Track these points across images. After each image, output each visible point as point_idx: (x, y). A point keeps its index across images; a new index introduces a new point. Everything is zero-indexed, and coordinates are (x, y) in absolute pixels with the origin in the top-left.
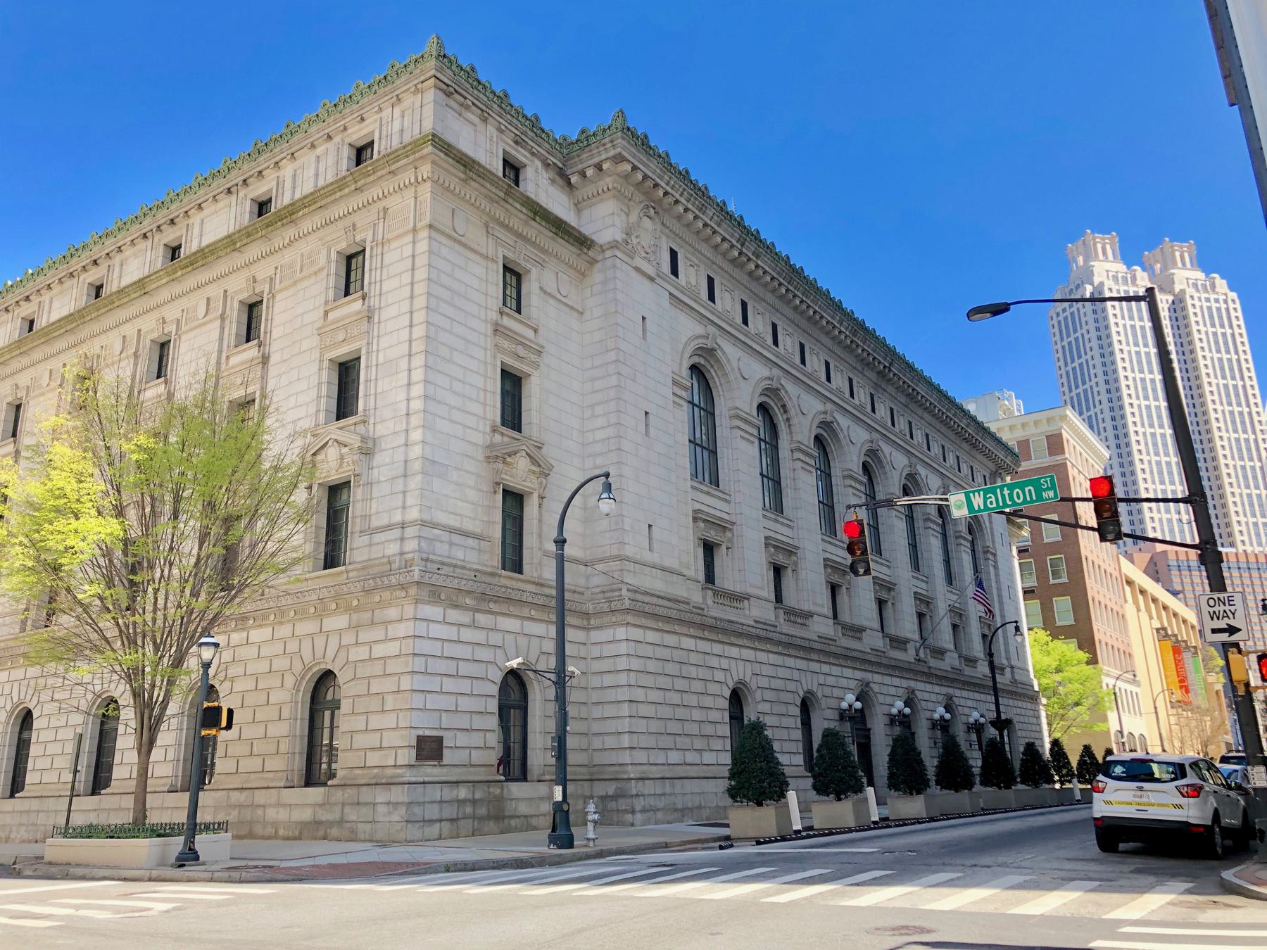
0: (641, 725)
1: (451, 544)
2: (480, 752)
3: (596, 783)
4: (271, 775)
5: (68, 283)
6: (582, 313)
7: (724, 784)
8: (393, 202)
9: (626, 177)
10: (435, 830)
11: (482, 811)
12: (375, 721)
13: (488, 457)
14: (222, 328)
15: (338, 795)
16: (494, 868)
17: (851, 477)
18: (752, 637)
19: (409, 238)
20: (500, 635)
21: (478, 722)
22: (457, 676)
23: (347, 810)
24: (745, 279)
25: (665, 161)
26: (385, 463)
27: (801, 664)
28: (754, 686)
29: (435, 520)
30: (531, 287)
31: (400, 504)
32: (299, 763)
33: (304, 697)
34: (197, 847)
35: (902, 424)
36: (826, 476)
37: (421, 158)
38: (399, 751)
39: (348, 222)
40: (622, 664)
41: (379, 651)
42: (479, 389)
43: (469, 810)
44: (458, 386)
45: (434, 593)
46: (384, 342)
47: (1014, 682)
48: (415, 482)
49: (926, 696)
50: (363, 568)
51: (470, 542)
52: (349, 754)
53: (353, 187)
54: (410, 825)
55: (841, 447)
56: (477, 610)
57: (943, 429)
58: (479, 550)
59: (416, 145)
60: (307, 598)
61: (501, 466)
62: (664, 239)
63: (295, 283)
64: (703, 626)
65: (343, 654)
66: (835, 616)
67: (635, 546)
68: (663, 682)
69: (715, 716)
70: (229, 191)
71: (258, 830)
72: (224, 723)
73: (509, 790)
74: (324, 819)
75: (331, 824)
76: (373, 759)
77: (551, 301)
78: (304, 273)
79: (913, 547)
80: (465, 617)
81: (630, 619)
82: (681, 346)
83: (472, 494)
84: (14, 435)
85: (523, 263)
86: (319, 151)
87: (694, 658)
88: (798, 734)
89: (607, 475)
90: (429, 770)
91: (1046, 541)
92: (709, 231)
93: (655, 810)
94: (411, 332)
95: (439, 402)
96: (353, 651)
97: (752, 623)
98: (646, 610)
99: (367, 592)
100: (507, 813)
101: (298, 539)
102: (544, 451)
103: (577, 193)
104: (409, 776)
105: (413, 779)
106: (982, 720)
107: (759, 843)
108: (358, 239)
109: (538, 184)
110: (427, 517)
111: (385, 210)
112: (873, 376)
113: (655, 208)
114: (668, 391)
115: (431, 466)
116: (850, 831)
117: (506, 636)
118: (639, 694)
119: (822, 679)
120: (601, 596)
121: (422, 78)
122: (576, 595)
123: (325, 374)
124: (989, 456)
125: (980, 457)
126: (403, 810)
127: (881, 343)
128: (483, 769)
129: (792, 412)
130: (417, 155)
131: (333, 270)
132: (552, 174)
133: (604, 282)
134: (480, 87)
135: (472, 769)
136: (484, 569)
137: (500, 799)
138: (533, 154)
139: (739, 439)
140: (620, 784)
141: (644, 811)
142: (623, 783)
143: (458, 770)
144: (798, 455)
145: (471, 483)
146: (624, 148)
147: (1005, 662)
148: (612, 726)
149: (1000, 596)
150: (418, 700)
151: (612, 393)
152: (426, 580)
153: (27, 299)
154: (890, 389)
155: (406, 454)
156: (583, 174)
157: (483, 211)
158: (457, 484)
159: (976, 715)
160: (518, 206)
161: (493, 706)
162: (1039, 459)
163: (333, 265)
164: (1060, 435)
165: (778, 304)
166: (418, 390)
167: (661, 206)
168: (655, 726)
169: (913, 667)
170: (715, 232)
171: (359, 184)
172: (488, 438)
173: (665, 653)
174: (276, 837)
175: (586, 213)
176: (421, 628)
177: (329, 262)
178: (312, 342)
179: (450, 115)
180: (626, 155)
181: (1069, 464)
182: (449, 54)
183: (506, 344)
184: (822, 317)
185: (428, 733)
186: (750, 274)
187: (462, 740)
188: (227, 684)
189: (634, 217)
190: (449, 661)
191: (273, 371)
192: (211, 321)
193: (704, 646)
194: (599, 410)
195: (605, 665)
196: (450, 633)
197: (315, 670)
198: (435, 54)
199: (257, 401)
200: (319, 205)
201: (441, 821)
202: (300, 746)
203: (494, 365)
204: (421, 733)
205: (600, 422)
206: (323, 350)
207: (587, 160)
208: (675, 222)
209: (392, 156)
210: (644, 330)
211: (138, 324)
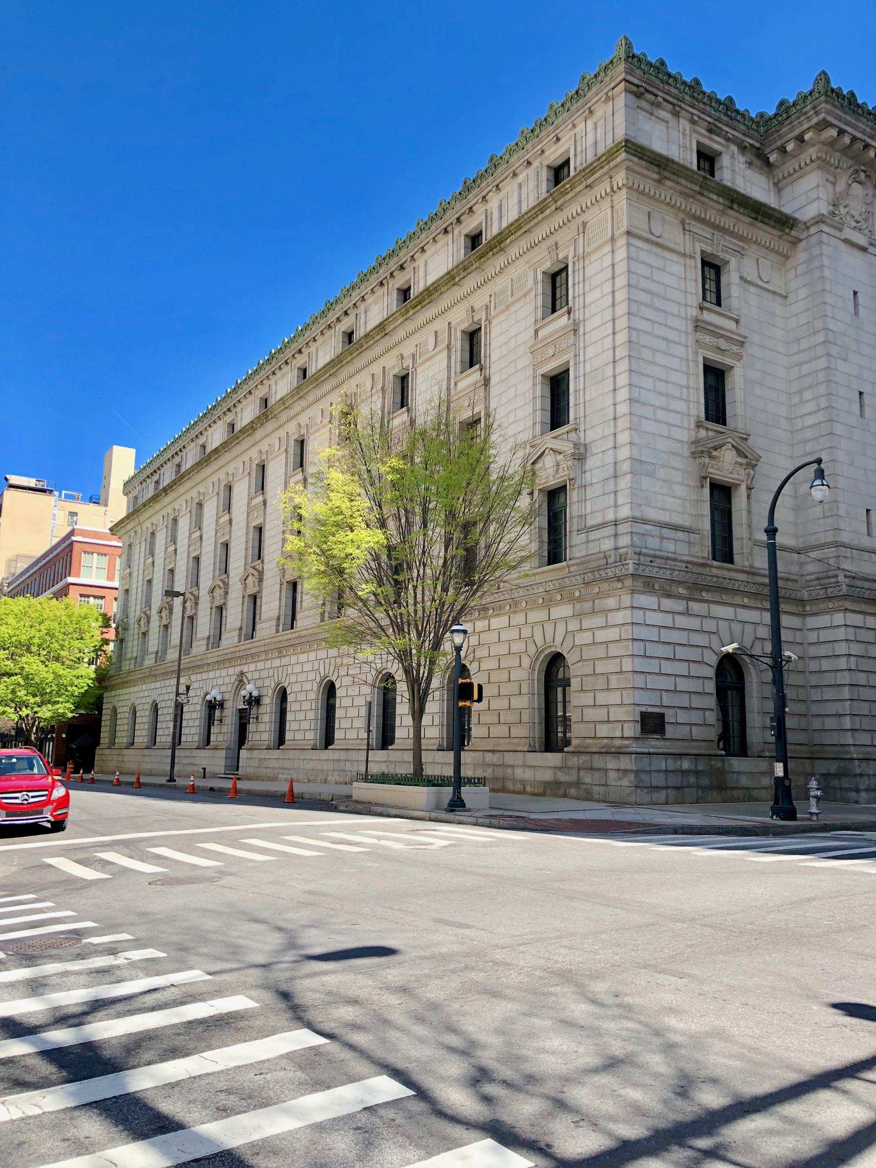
1: (662, 538)
2: (700, 729)
3: (817, 762)
5: (328, 333)
6: (786, 297)
9: (831, 144)
10: (662, 796)
11: (705, 781)
12: (602, 698)
14: (449, 357)
15: (574, 761)
19: (608, 248)
20: (714, 622)
21: (697, 702)
22: (674, 659)
26: (597, 467)
29: (646, 516)
30: (731, 279)
31: (612, 503)
32: (538, 732)
33: (538, 677)
34: (463, 796)
37: (616, 166)
38: (625, 725)
39: (551, 241)
40: (842, 649)
41: (601, 636)
42: (682, 386)
43: (692, 780)
44: (661, 386)
45: (648, 585)
48: (625, 482)
50: (582, 563)
51: (680, 535)
52: (581, 726)
53: (553, 208)
54: (638, 791)
56: (691, 599)
58: (689, 543)
60: (536, 591)
61: (707, 460)
63: (508, 307)
65: (569, 638)
70: (446, 231)
71: (510, 785)
73: (730, 765)
75: (570, 785)
77: (753, 289)
78: (515, 297)
80: (680, 606)
81: (848, 605)
83: (679, 490)
84: (302, 465)
85: (722, 255)
86: (521, 178)
89: (819, 461)
94: (614, 339)
95: (643, 404)
98: (866, 595)
99: (587, 584)
100: (729, 785)
101: (523, 539)
102: (751, 442)
104: (635, 747)
105: (639, 750)
108: (561, 256)
110: (638, 514)
111: (584, 224)
115: (639, 467)
118: (861, 679)
121: (612, 85)
122: (790, 583)
123: (539, 388)
126: (632, 777)
128: (703, 744)
130: (612, 164)
131: (540, 290)
132: (749, 156)
133: (809, 261)
136: (695, 560)
137: (721, 773)
138: (728, 140)
140: (842, 764)
142: (847, 762)
145: (679, 479)
146: (828, 112)
150: (639, 681)
151: (821, 376)
152: (640, 572)
153: (300, 351)
155: (615, 456)
156: (783, 150)
157: (679, 209)
158: (664, 481)
160: (715, 197)
166: (623, 394)
172: (693, 433)
174: (523, 792)
175: (786, 192)
177: (536, 283)
178: (525, 361)
179: (642, 116)
180: (830, 119)
182: (637, 52)
183: (708, 339)
185: (650, 710)
187: (683, 717)
189: (841, 186)
190: (667, 646)
191: (494, 391)
192: (441, 351)
194: (807, 395)
195: (823, 650)
196: (667, 620)
197: (546, 652)
198: (623, 56)
199: (482, 420)
200: (523, 230)
203: (696, 362)
204: (644, 709)
205: (809, 407)
206: (535, 367)
209: (590, 170)
210: (856, 305)
211: (382, 362)
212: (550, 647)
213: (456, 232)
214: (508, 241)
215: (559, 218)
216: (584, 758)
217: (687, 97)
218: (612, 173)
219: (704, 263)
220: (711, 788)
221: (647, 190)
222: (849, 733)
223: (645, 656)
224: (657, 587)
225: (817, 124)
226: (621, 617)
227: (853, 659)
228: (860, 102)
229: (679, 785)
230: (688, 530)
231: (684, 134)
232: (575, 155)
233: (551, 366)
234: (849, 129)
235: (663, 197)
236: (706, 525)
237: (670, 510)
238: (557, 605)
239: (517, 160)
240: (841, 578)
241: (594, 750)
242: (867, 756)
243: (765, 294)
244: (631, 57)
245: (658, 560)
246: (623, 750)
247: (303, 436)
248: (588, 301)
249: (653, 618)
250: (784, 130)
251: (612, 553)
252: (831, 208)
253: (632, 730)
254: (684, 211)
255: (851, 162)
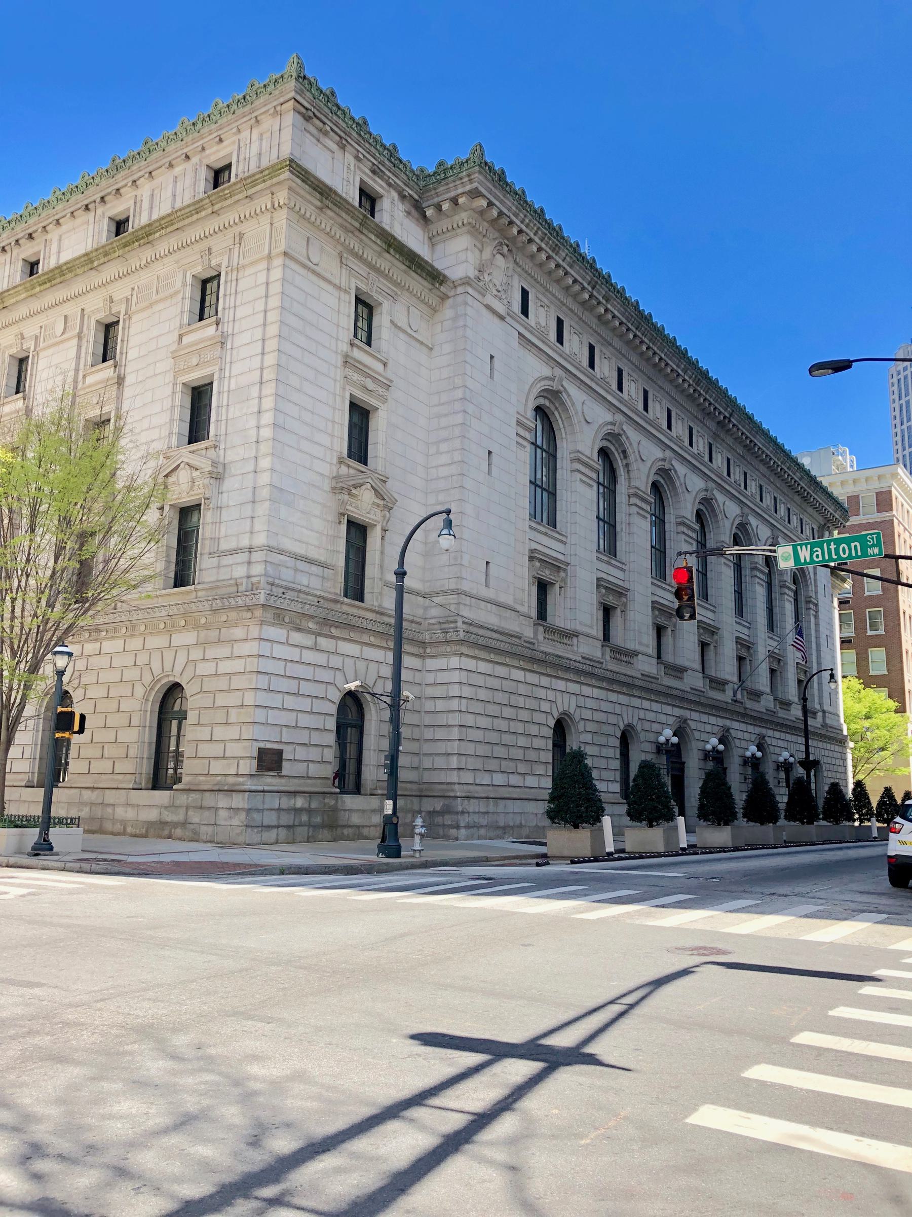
0: (470, 749)
1: (296, 570)
2: (318, 765)
3: (425, 800)
4: (120, 777)
6: (431, 349)
7: (543, 807)
8: (249, 228)
9: (482, 213)
10: (272, 835)
11: (318, 820)
13: (334, 488)
14: (79, 347)
15: (183, 799)
16: (325, 873)
17: (684, 524)
18: (579, 672)
21: (316, 738)
22: (298, 694)
23: (191, 813)
24: (594, 322)
25: (520, 197)
27: (623, 699)
28: (577, 717)
29: (281, 546)
30: (382, 321)
31: (248, 529)
32: (147, 768)
35: (737, 475)
36: (660, 522)
37: (279, 183)
39: (205, 245)
40: (455, 691)
43: (304, 818)
45: (279, 616)
46: (237, 368)
47: (825, 725)
49: (740, 735)
50: (212, 589)
51: (314, 569)
53: (210, 211)
54: (249, 830)
55: (676, 494)
56: (320, 634)
57: (778, 482)
58: (323, 577)
59: (274, 170)
60: (158, 614)
61: (346, 497)
62: (516, 277)
63: (151, 306)
64: (533, 660)
66: (659, 656)
67: (473, 582)
68: (492, 709)
69: (538, 743)
71: (108, 826)
72: (76, 728)
73: (343, 802)
74: (169, 819)
75: (175, 825)
76: (217, 767)
77: (402, 335)
78: (160, 296)
79: (739, 594)
80: (308, 640)
81: (464, 649)
82: (527, 387)
86: (178, 170)
87: (522, 689)
88: (616, 764)
89: (448, 512)
90: (269, 780)
91: (867, 594)
92: (561, 272)
93: (480, 827)
96: (200, 666)
97: (580, 659)
100: (341, 823)
101: (146, 556)
103: (431, 227)
104: (250, 785)
105: (254, 788)
106: (792, 760)
107: (573, 862)
108: (213, 263)
109: (394, 216)
110: (274, 544)
111: (241, 235)
112: (712, 425)
113: (509, 245)
114: (512, 430)
115: (280, 494)
116: (659, 855)
117: (347, 660)
118: (469, 720)
119: (642, 714)
120: (436, 627)
121: (282, 100)
122: (413, 625)
123: (178, 396)
124: (819, 510)
125: (810, 510)
126: (243, 815)
127: (724, 393)
128: (319, 781)
129: (632, 458)
130: (275, 180)
131: (188, 294)
132: (408, 206)
133: (455, 319)
134: (339, 113)
135: (309, 781)
136: (327, 595)
137: (334, 810)
138: (390, 185)
139: (578, 483)
140: (447, 802)
141: (468, 827)
143: (296, 781)
144: (634, 500)
147: (817, 707)
148: (442, 748)
149: (818, 645)
150: (260, 716)
151: (457, 431)
152: (271, 603)
154: (730, 441)
155: (255, 481)
157: (338, 241)
159: (786, 754)
160: (373, 238)
161: (331, 724)
162: (867, 514)
163: (188, 289)
164: (890, 492)
165: (625, 349)
166: (268, 418)
167: (514, 243)
168: (482, 750)
169: (730, 707)
170: (566, 273)
171: (216, 207)
172: (335, 469)
173: (496, 683)
174: (124, 833)
175: (439, 247)
176: (266, 649)
177: (184, 284)
179: (309, 140)
181: (896, 521)
183: (356, 376)
184: (667, 364)
185: (269, 746)
186: (600, 317)
187: (301, 753)
188: (80, 691)
190: (291, 680)
191: (128, 392)
193: (532, 678)
194: (444, 447)
195: (438, 691)
196: (294, 654)
197: (163, 682)
198: (295, 75)
199: (112, 421)
200: (175, 227)
201: (278, 827)
202: (148, 752)
203: (343, 397)
204: (262, 745)
205: (444, 459)
206: (177, 374)
207: (444, 194)
208: (528, 261)
212: (168, 676)
213: (99, 212)
214: (157, 235)
215: (214, 224)
216: (193, 796)
217: (354, 134)
218: (274, 189)
219: (358, 300)
220: (323, 826)
221: (308, 215)
222: (455, 772)
223: (269, 690)
224: (287, 620)
225: (470, 191)
226: (251, 648)
227: (464, 701)
228: (509, 181)
229: (291, 823)
230: (323, 565)
231: (348, 168)
232: (238, 162)
233: (195, 376)
234: (497, 203)
235: (323, 226)
236: (341, 562)
237: (307, 543)
238: (179, 631)
239: (175, 150)
240: (460, 624)
241: (205, 788)
242: (469, 794)
243: (414, 343)
244: (302, 78)
245: (290, 592)
246: (237, 788)
247: (28, 350)
248: (238, 315)
249: (280, 651)
250: (442, 189)
251: (244, 580)
252: (477, 273)
253: (248, 766)
254: (342, 244)
255: (497, 235)
